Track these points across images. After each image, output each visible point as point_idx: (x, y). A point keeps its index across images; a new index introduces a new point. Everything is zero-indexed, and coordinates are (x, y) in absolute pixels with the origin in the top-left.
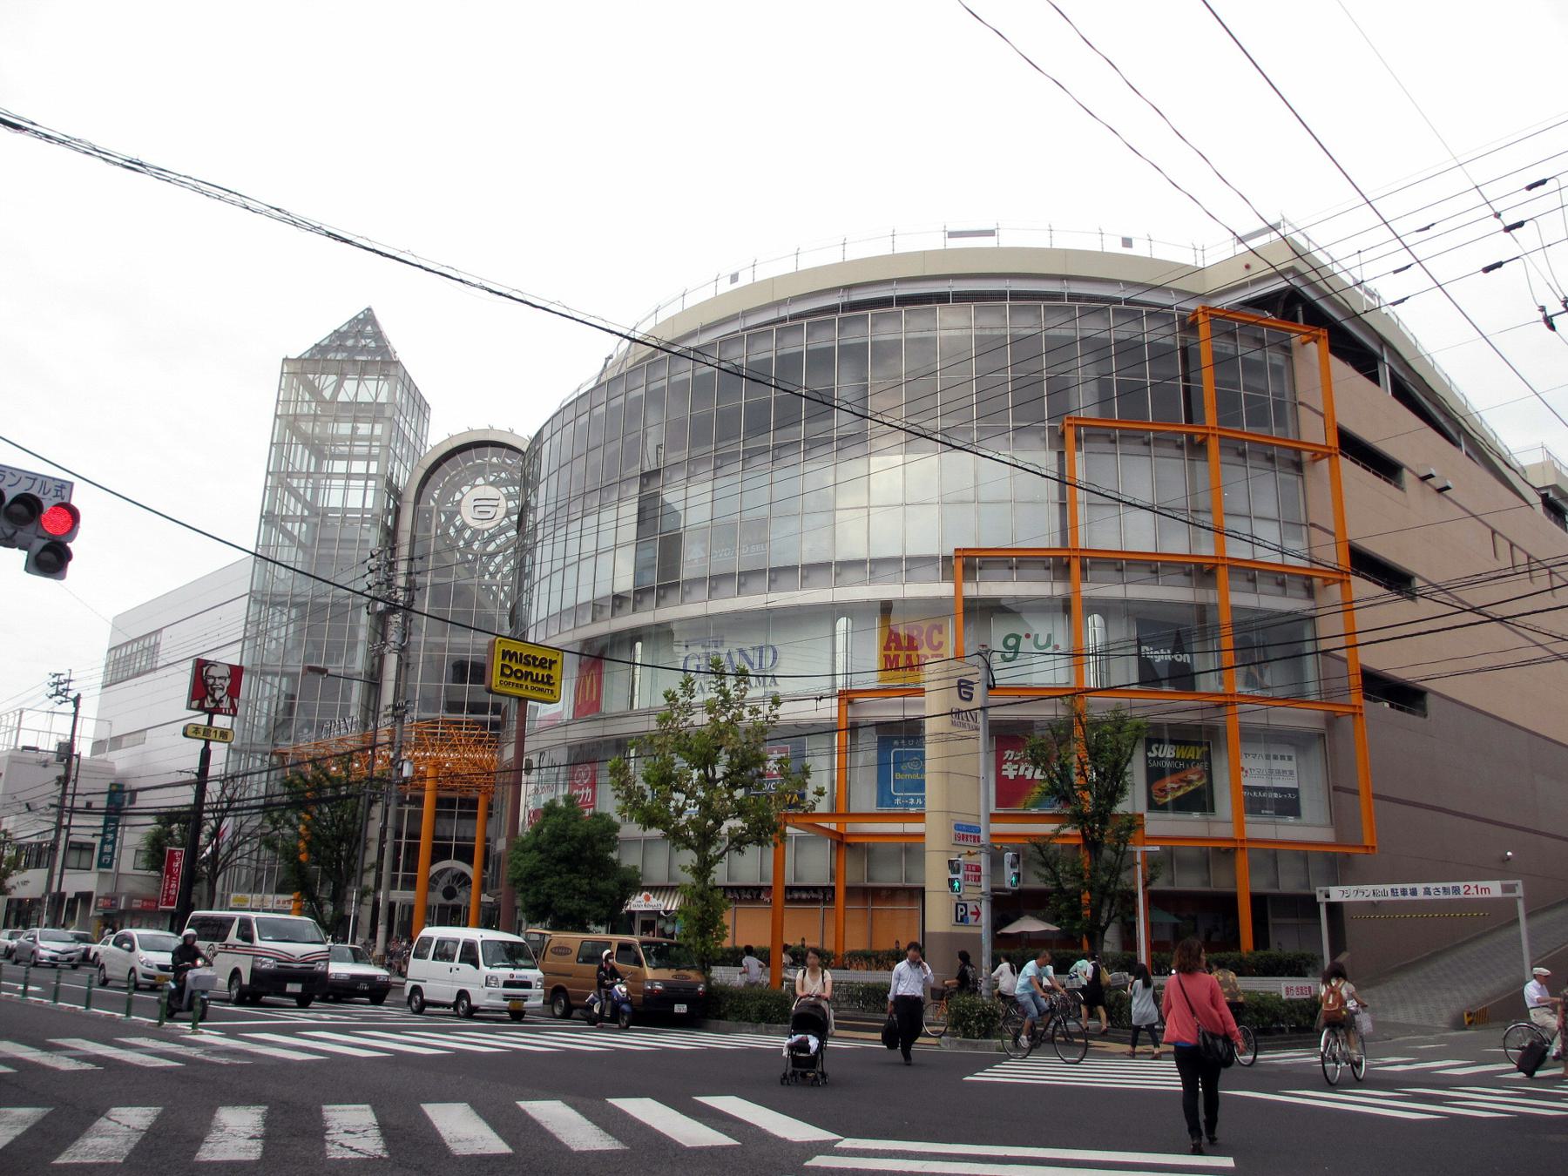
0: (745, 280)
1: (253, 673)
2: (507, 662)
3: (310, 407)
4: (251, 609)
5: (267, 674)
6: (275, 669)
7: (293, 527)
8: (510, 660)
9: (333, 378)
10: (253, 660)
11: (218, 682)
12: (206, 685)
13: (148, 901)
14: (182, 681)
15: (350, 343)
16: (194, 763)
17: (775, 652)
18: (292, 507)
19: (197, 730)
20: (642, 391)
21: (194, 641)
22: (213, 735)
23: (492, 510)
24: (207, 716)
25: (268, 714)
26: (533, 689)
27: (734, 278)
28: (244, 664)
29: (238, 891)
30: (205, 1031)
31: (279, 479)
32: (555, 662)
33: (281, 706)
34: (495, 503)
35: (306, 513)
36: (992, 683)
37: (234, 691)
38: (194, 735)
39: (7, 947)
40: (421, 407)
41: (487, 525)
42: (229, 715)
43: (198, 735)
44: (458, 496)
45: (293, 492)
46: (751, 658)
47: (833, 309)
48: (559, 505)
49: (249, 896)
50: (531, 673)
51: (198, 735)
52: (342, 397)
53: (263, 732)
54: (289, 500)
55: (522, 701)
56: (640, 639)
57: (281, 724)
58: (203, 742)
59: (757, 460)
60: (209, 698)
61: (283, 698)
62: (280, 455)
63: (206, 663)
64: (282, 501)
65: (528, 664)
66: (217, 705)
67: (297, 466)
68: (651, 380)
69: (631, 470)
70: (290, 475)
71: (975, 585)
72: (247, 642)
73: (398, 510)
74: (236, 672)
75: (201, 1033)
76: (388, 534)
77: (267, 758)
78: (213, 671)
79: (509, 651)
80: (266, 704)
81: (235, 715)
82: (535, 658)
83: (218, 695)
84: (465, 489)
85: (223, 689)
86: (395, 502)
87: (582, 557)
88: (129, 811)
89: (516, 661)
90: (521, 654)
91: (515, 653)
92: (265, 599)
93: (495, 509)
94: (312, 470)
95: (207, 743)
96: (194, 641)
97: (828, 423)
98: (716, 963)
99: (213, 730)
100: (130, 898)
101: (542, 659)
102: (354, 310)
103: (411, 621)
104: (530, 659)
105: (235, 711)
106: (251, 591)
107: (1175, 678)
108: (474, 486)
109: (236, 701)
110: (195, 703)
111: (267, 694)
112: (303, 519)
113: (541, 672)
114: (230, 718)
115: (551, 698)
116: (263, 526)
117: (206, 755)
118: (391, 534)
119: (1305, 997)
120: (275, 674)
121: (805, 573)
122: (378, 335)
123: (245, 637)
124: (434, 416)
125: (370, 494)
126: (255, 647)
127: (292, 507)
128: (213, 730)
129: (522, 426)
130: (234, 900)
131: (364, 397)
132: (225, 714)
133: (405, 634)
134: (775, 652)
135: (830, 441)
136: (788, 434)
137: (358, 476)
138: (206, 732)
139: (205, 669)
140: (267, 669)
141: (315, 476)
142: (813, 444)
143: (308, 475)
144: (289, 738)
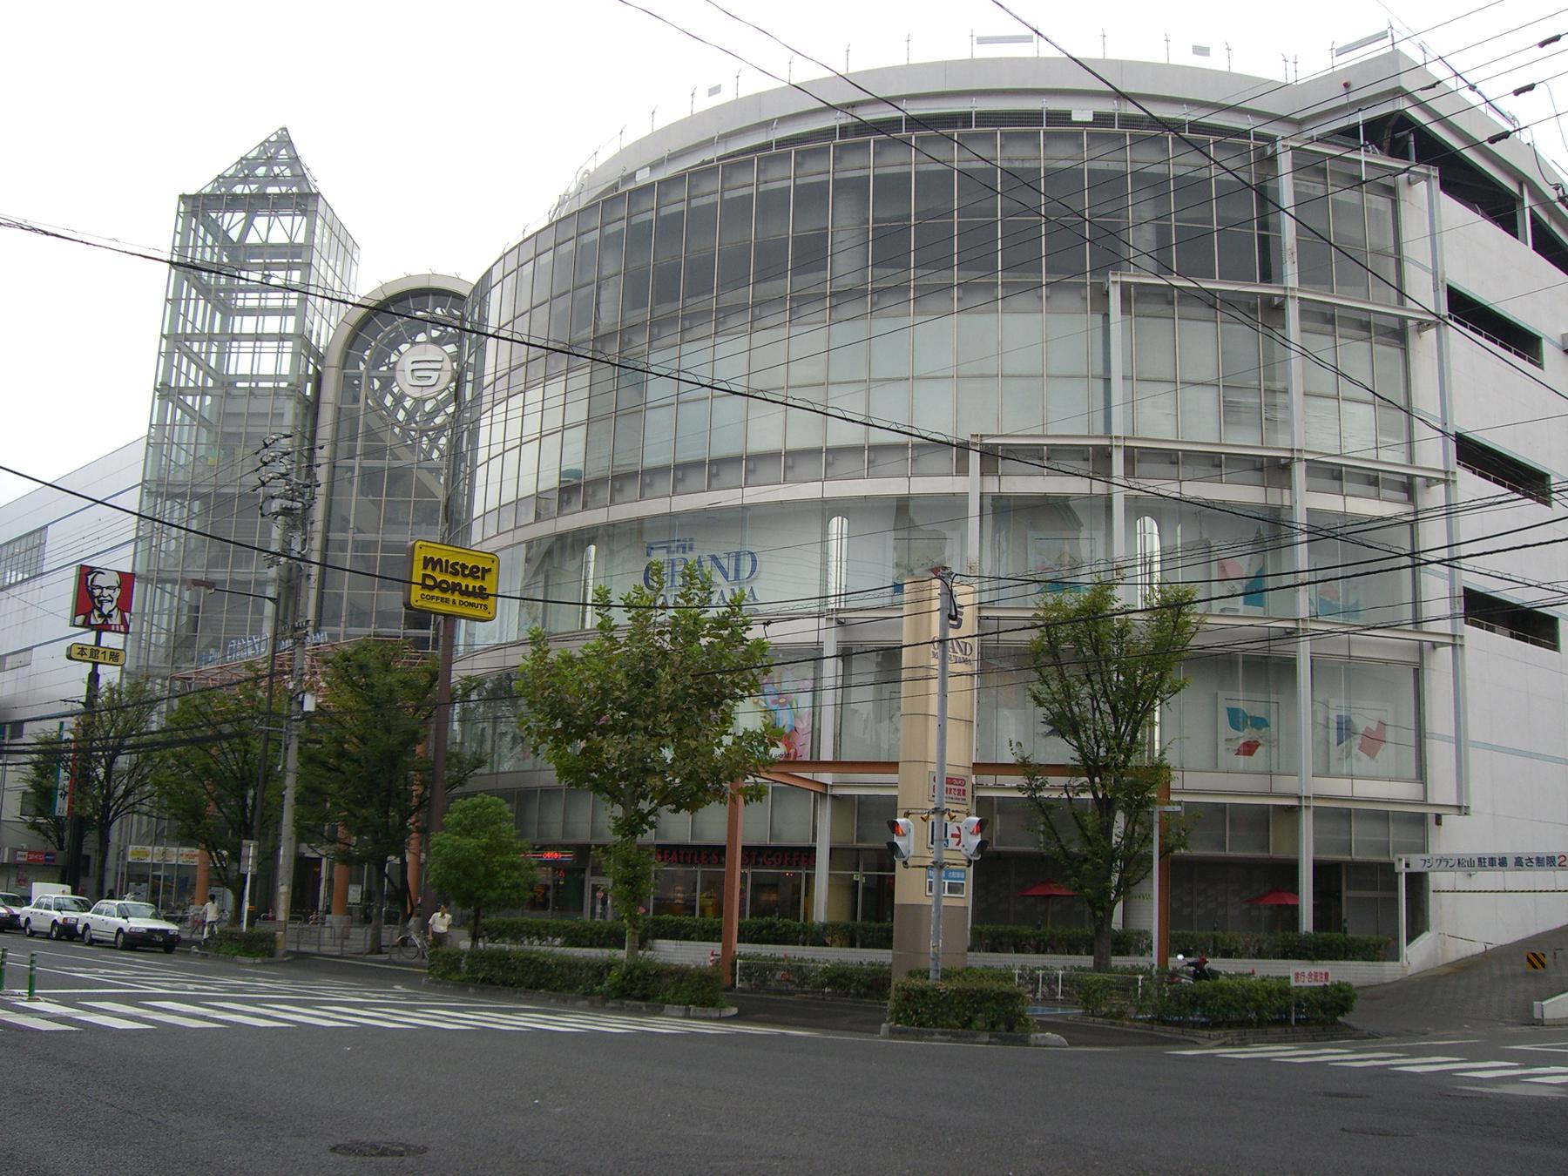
0: (726, 96)
1: (148, 580)
2: (429, 572)
3: (213, 252)
4: (144, 503)
5: (165, 581)
6: (175, 575)
7: (194, 401)
8: (434, 569)
9: (240, 216)
10: (148, 566)
11: (106, 593)
12: (91, 594)
13: (35, 853)
14: (62, 590)
15: (261, 171)
16: (81, 691)
17: (754, 561)
18: (192, 376)
19: (82, 651)
20: (596, 235)
21: (63, 549)
22: (101, 656)
23: (435, 375)
24: (94, 633)
25: (168, 630)
26: (462, 603)
27: (714, 91)
28: (137, 569)
29: (138, 843)
30: (41, 999)
31: (176, 342)
32: (490, 570)
33: (184, 619)
34: (438, 366)
35: (210, 383)
36: (954, 613)
37: (124, 604)
38: (79, 657)
39: (120, 930)
40: (345, 245)
41: (427, 393)
42: (120, 632)
43: (85, 657)
44: (393, 358)
45: (193, 358)
46: (725, 566)
47: (828, 133)
48: (498, 375)
49: (150, 848)
50: (459, 584)
51: (85, 657)
52: (252, 238)
53: (162, 651)
54: (188, 367)
55: (451, 619)
56: (592, 541)
57: (182, 644)
58: (90, 665)
59: (733, 321)
60: (96, 613)
61: (185, 610)
62: (175, 314)
63: (92, 570)
64: (179, 368)
65: (456, 573)
66: (106, 620)
67: (199, 325)
68: (607, 220)
69: (582, 333)
70: (187, 337)
71: (996, 478)
72: (140, 543)
73: (318, 380)
74: (127, 580)
75: (38, 1000)
76: (307, 407)
77: (167, 683)
78: (100, 580)
79: (432, 558)
80: (165, 617)
81: (126, 633)
82: (464, 566)
83: (107, 608)
84: (404, 348)
85: (112, 601)
86: (315, 368)
87: (524, 440)
88: (12, 748)
89: (441, 571)
90: (447, 561)
91: (440, 561)
92: (161, 490)
93: (437, 373)
94: (217, 330)
95: (95, 665)
96: (63, 549)
97: (821, 275)
98: (664, 936)
99: (102, 650)
100: (14, 852)
101: (473, 567)
102: (266, 130)
103: (312, 523)
104: (458, 567)
105: (127, 627)
106: (144, 481)
107: (1248, 594)
108: (414, 343)
109: (127, 615)
110: (80, 619)
111: (166, 605)
112: (204, 391)
113: (471, 583)
114: (123, 635)
115: (485, 615)
116: (157, 401)
117: (94, 677)
118: (312, 408)
119: (1316, 984)
120: (174, 582)
121: (790, 462)
122: (295, 161)
123: (137, 537)
124: (364, 257)
125: (287, 358)
126: (150, 549)
127: (192, 376)
128: (102, 650)
129: (463, 269)
130: (133, 854)
131: (278, 237)
132: (115, 631)
133: (305, 540)
134: (754, 561)
135: (823, 297)
136: (771, 288)
137: (270, 337)
138: (94, 653)
139: (90, 577)
140: (165, 575)
141: (219, 338)
142: (800, 301)
143: (211, 338)
144: (193, 660)
